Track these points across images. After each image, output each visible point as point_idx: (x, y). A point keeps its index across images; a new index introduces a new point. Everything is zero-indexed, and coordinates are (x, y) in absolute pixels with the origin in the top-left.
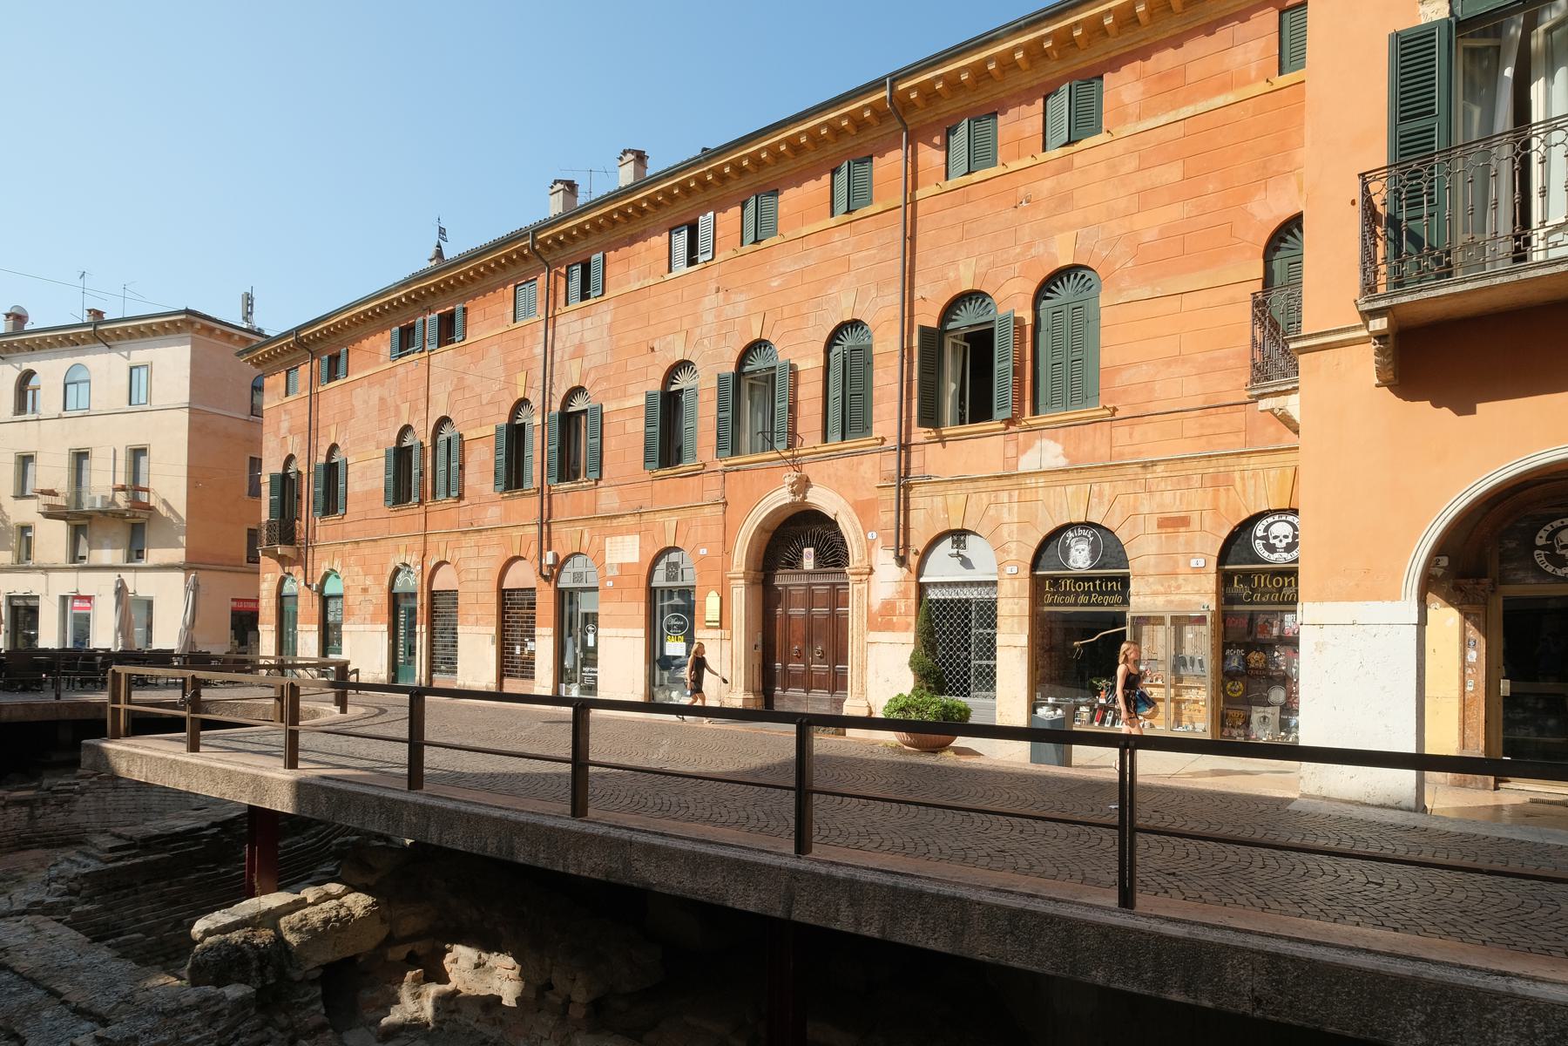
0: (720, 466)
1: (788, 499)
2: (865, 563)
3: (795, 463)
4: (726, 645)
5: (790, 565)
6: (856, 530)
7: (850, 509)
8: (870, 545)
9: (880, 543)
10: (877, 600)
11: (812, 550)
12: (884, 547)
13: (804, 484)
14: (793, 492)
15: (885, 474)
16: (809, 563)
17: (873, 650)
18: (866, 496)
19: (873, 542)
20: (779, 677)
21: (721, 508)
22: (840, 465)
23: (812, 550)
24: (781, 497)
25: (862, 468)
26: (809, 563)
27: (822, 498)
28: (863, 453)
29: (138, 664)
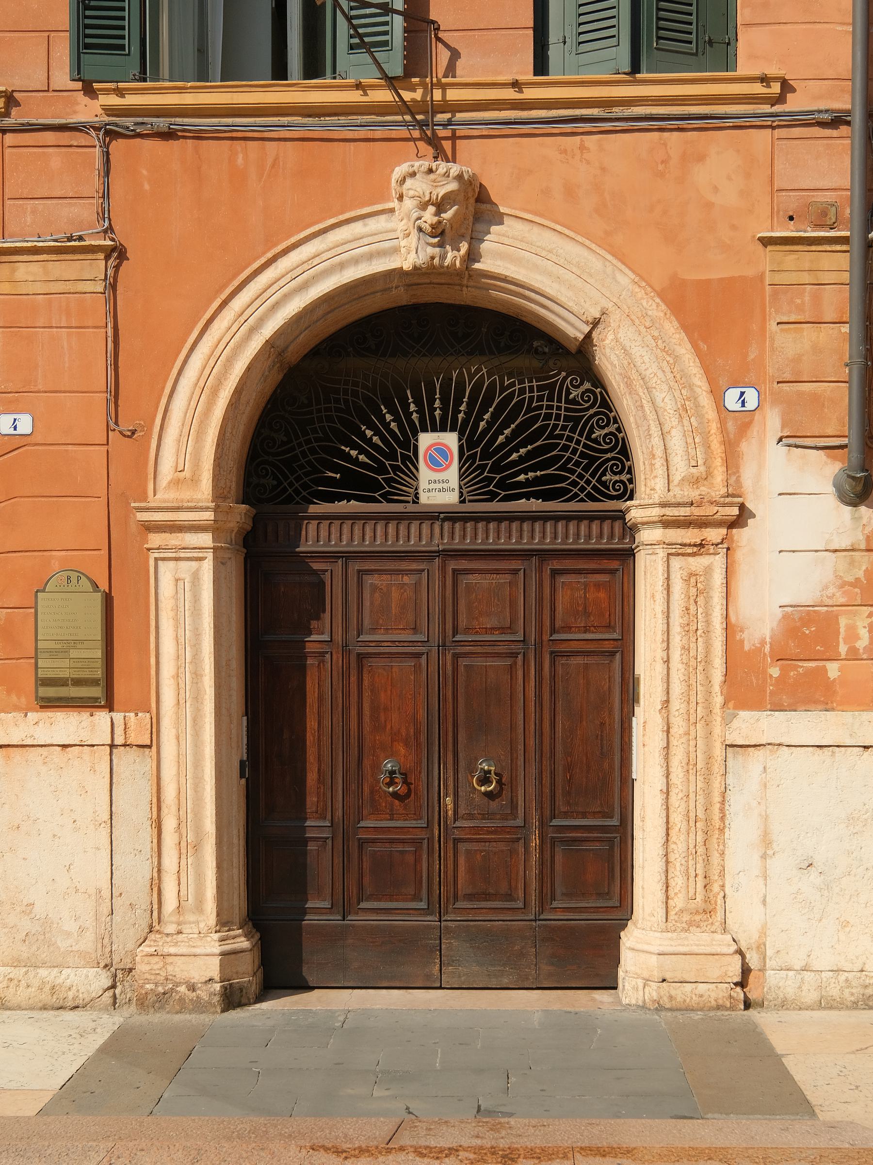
0: (88, 110)
1: (411, 253)
2: (718, 487)
3: (433, 129)
4: (133, 767)
5: (361, 485)
6: (682, 381)
7: (655, 308)
8: (736, 429)
9: (773, 422)
10: (762, 609)
11: (451, 440)
12: (792, 439)
13: (473, 210)
14: (440, 233)
15: (791, 202)
16: (439, 477)
17: (747, 777)
18: (719, 269)
19: (745, 421)
20: (322, 861)
21: (97, 267)
22: (618, 155)
23: (451, 440)
24: (378, 236)
25: (703, 176)
26: (439, 477)
27: (541, 263)
28: (708, 123)
29: (523, 109)
